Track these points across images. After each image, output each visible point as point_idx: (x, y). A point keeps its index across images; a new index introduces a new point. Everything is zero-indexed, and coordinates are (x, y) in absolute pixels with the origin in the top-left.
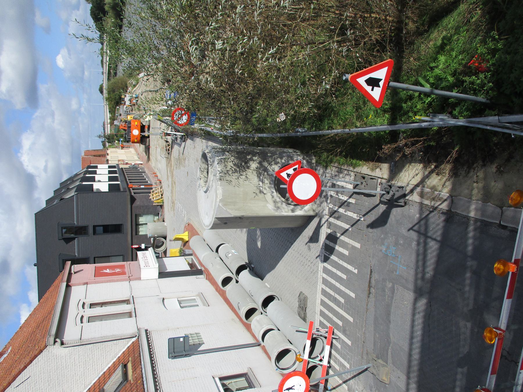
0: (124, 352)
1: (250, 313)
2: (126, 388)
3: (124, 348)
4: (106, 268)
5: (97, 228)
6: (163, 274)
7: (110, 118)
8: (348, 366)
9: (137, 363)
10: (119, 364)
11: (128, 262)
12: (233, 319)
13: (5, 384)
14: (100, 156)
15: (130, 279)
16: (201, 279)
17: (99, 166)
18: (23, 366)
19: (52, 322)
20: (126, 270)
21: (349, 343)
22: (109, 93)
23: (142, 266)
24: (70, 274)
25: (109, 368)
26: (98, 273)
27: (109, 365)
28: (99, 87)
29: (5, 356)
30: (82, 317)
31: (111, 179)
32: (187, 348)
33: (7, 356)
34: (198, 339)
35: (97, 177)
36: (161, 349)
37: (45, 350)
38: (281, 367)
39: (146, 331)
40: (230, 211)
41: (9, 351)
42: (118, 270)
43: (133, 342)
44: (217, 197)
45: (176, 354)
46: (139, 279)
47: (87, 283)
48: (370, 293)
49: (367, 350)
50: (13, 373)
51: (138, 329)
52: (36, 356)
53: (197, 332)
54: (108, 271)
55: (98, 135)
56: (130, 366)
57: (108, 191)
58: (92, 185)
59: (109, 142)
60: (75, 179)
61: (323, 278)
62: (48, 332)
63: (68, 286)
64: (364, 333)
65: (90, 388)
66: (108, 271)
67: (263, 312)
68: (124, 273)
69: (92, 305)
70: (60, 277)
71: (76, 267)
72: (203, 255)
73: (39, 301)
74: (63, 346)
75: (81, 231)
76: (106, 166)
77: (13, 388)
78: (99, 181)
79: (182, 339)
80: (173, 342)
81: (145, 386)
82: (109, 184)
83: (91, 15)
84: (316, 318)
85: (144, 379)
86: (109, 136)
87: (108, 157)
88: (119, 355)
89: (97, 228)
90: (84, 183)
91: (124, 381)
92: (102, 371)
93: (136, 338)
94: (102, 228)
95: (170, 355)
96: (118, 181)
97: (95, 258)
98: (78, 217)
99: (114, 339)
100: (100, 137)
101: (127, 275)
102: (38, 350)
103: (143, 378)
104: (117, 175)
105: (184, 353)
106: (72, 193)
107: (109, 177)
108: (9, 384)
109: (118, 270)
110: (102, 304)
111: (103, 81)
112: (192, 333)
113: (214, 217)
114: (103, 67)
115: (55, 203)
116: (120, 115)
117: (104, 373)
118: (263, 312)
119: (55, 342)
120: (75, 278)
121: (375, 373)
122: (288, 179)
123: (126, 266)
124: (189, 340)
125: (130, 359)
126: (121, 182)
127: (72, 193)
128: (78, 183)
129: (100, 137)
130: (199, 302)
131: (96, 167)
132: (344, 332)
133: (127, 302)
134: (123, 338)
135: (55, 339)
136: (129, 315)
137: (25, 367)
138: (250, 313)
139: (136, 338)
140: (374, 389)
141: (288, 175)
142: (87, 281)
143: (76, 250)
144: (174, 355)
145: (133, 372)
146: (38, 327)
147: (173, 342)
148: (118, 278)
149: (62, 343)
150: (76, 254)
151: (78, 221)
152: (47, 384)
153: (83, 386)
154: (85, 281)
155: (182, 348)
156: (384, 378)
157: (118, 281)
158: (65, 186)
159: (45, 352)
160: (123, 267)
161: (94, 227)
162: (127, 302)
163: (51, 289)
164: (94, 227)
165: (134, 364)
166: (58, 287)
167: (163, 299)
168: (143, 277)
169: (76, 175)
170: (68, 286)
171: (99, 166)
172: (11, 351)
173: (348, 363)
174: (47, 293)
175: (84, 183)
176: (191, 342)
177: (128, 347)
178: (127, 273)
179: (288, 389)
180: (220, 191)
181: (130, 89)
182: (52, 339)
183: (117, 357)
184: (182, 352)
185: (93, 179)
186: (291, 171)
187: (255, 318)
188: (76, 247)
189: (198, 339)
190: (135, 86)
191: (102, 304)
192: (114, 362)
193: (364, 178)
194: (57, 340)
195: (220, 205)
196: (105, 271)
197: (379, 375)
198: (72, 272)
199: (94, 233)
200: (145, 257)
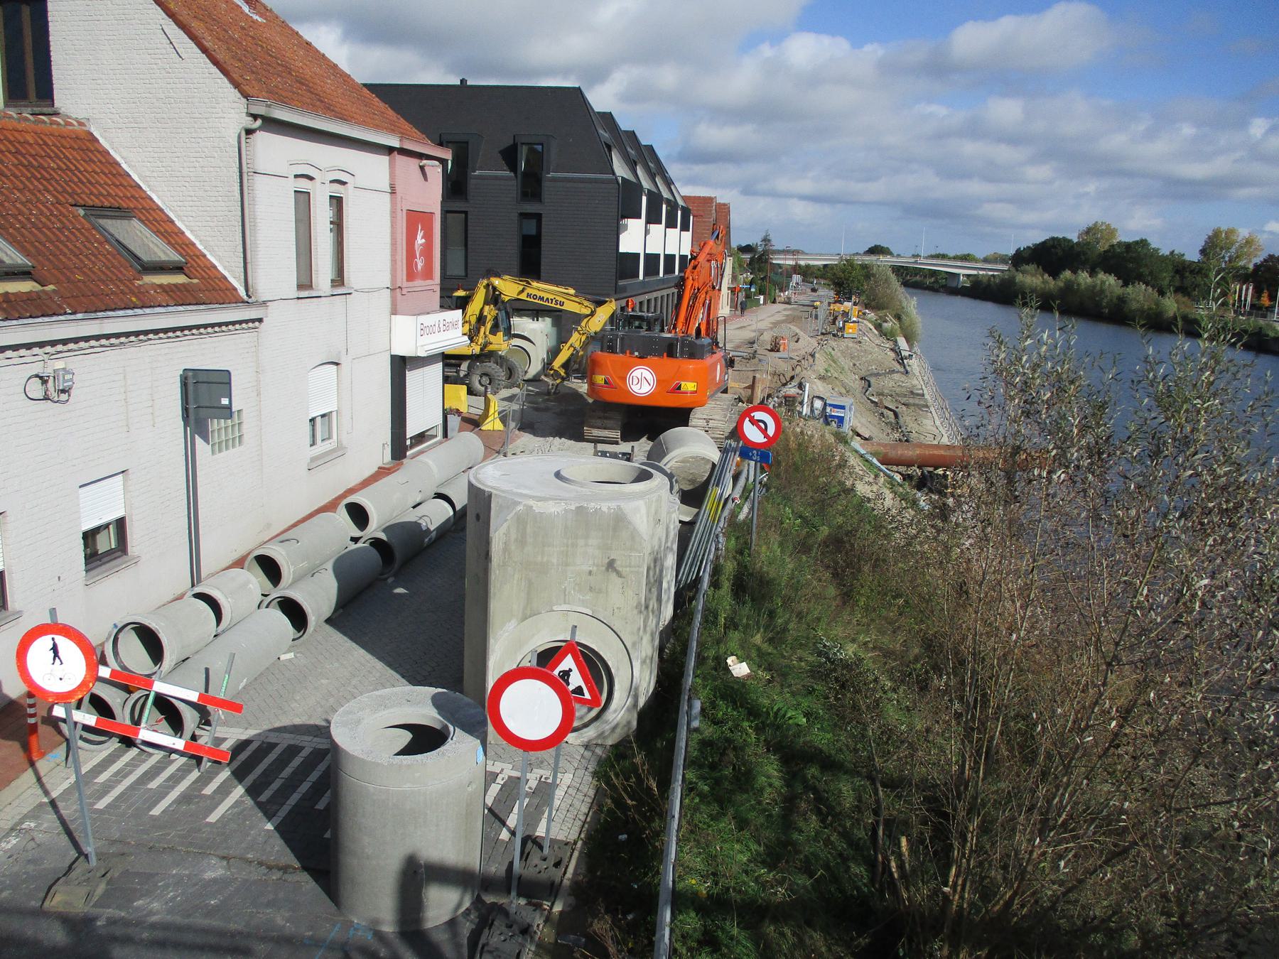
0: (215, 267)
1: (270, 568)
2: (126, 268)
3: (225, 268)
4: (428, 236)
5: (534, 222)
6: (401, 365)
7: (808, 266)
8: (101, 805)
9: (181, 297)
10: (188, 254)
11: (438, 289)
12: (269, 526)
13: (172, 6)
16: (384, 456)
17: (687, 236)
18: (208, 44)
20: (419, 283)
21: (156, 811)
22: (864, 266)
23: (429, 320)
24: (421, 156)
25: (183, 233)
26: (416, 219)
27: (188, 234)
28: (885, 245)
29: (246, 9)
30: (311, 179)
31: (652, 259)
32: (203, 412)
33: (242, 12)
34: (227, 441)
35: (657, 229)
36: (205, 354)
37: (239, 95)
38: (121, 636)
39: (260, 320)
40: (503, 530)
41: (255, 17)
42: (420, 264)
43: (235, 289)
44: (540, 499)
45: (191, 388)
46: (394, 312)
47: (393, 192)
48: (270, 868)
49: (131, 854)
50: (195, 25)
51: (264, 302)
52: (225, 72)
53: (245, 438)
54: (420, 240)
55: (771, 237)
56: (180, 279)
57: (622, 250)
59: (752, 259)
60: (658, 179)
61: (275, 745)
62: (285, 102)
63: (390, 150)
64: (172, 849)
65: (140, 187)
66: (420, 240)
67: (269, 599)
68: (411, 276)
69: (337, 202)
70: (416, 132)
71: (435, 171)
72: (430, 462)
73: (365, 85)
74: (243, 133)
75: (532, 185)
77: (162, 22)
78: (647, 232)
79: (225, 401)
80: (222, 380)
81: (121, 313)
82: (638, 255)
83: (1053, 239)
84: (232, 730)
85: (139, 311)
86: (766, 261)
88: (209, 256)
89: (534, 222)
90: (644, 199)
91: (142, 266)
92: (178, 216)
93: (245, 298)
94: (534, 232)
95: (190, 374)
96: (665, 273)
97: (466, 213)
98: (596, 181)
99: (248, 247)
100: (766, 240)
101: (405, 284)
102: (240, 80)
103: (142, 307)
104: (661, 274)
105: (192, 406)
106: (620, 169)
108: (171, 14)
109: (420, 264)
110: (338, 225)
111: (898, 256)
112: (244, 426)
113: (494, 492)
114: (932, 257)
115: (601, 131)
116: (814, 290)
117: (172, 222)
118: (269, 599)
119: (255, 117)
120: (409, 166)
121: (73, 875)
122: (556, 672)
123: (429, 282)
124: (219, 418)
125: (195, 281)
126: (643, 282)
127: (620, 169)
128: (646, 184)
129: (766, 240)
130: (321, 447)
131: (685, 227)
132: (185, 798)
133: (339, 279)
134: (249, 266)
135: (262, 117)
136: (305, 284)
137: (204, 50)
138: (270, 568)
139: (245, 298)
140: (31, 868)
141: (566, 674)
142: (399, 195)
143: (559, 175)
144: (191, 381)
145: (161, 286)
146: (301, 82)
147: (222, 380)
148: (399, 263)
149: (249, 132)
150: (477, 173)
151: (554, 180)
152: (162, 96)
153: (148, 174)
154: (398, 189)
155: (204, 400)
156: (58, 898)
157: (394, 261)
158: (644, 156)
159: (234, 93)
160: (428, 274)
161: (538, 217)
162: (339, 279)
163: (391, 112)
164: (538, 217)
165: (179, 290)
166: (392, 129)
167: (337, 364)
168: (398, 319)
169: (669, 183)
170: (390, 150)
171: (687, 236)
172: (254, 22)
173: (109, 806)
174: (381, 104)
175: (644, 199)
176: (214, 425)
177: (225, 278)
178: (411, 284)
179: (55, 649)
180: (552, 508)
181: (871, 315)
182: (260, 110)
183: (205, 252)
184: (196, 400)
185: (653, 218)
186: (576, 680)
187: (255, 580)
188: (490, 174)
189: (227, 441)
190: (878, 327)
191: (338, 225)
192: (194, 245)
193: (557, 865)
194: (259, 122)
195: (520, 508)
196: (420, 234)
197: (66, 883)
198: (425, 162)
199: (524, 216)
200: (447, 326)
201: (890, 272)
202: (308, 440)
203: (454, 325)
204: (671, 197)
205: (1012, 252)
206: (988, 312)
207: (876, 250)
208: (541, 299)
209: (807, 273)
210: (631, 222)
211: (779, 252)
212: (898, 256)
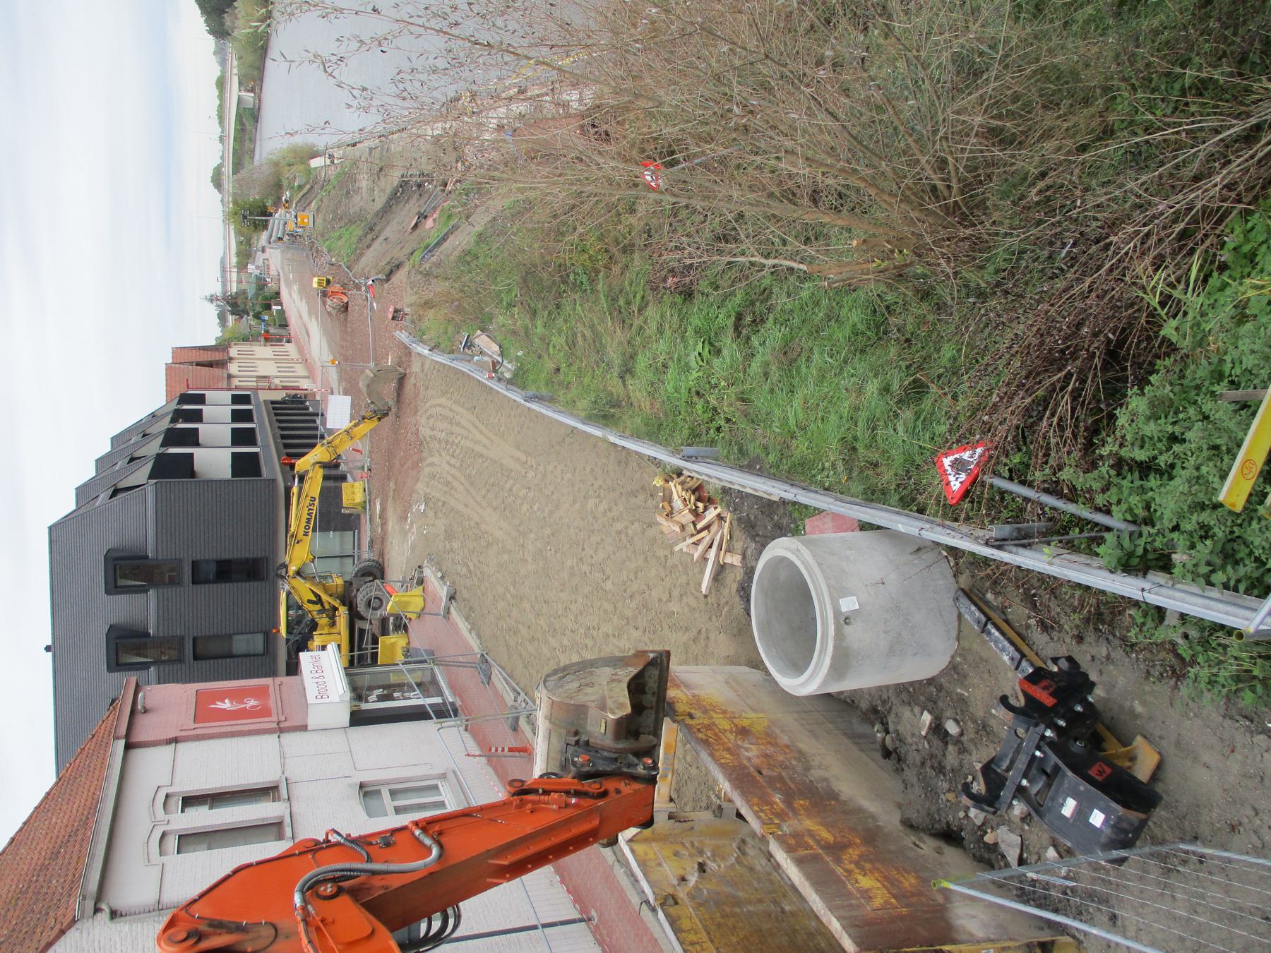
4: (221, 695)
7: (238, 254)
14: (210, 365)
15: (281, 730)
19: (92, 856)
20: (272, 703)
26: (203, 711)
37: (72, 930)
47: (175, 740)
54: (227, 705)
58: (191, 455)
59: (233, 313)
62: (76, 881)
66: (227, 705)
68: (264, 712)
69: (190, 801)
76: (227, 396)
87: (233, 368)
90: (185, 407)
100: (212, 299)
101: (274, 718)
102: (56, 930)
107: (233, 411)
110: (215, 799)
123: (271, 690)
129: (212, 299)
146: (55, 855)
149: (114, 914)
159: (72, 935)
160: (261, 693)
168: (311, 723)
175: (185, 407)
182: (90, 904)
191: (215, 799)
196: (220, 705)
200: (318, 669)
201: (163, 450)
202: (167, 869)
203: (316, 660)
204: (169, 418)
205: (210, 41)
206: (274, 70)
207: (217, 181)
208: (308, 521)
209: (245, 255)
210: (198, 465)
211: (224, 284)
212: (222, 158)
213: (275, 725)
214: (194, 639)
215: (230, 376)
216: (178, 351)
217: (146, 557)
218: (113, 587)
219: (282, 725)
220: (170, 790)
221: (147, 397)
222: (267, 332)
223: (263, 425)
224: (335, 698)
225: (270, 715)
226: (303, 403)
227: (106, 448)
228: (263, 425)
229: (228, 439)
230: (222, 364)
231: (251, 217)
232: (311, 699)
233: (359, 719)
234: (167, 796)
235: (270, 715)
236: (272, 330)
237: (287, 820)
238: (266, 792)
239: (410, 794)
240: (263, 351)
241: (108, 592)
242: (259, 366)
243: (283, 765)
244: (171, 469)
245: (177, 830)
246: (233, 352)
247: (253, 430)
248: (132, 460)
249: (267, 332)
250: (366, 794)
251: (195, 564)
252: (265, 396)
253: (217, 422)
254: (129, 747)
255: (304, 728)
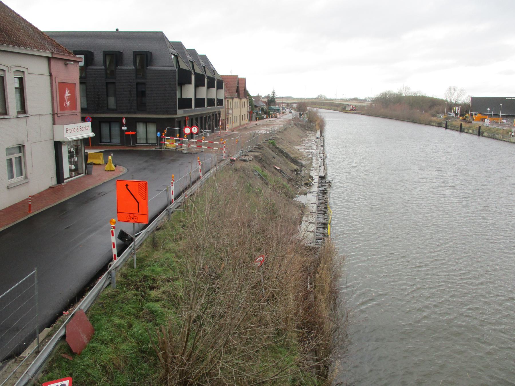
4: (73, 93)
15: (53, 115)
47: (51, 75)
58: (204, 86)
66: (67, 94)
68: (63, 108)
87: (236, 100)
100: (274, 93)
101: (59, 112)
107: (191, 99)
110: (21, 90)
129: (274, 93)
168: (56, 127)
200: (82, 129)
213: (56, 112)
214: (114, 83)
215: (233, 99)
216: (244, 80)
217: (117, 65)
218: (136, 54)
219: (56, 116)
220: (26, 73)
221: (222, 68)
222: (254, 113)
223: (207, 110)
224: (66, 135)
225: (61, 110)
226: (216, 127)
227: (200, 52)
228: (207, 110)
229: (210, 97)
230: (239, 96)
231: (302, 106)
232: (66, 126)
233: (58, 146)
234: (23, 72)
235: (61, 110)
236: (254, 114)
237: (6, 117)
238: (23, 109)
239: (18, 167)
240: (245, 111)
241: (134, 52)
242: (238, 110)
243: (35, 115)
244: (184, 77)
245: (5, 75)
246: (244, 100)
247: (204, 106)
248: (192, 62)
249: (254, 113)
250: (20, 148)
251: (144, 84)
252: (222, 111)
253: (214, 94)
254: (49, 59)
255: (54, 123)
